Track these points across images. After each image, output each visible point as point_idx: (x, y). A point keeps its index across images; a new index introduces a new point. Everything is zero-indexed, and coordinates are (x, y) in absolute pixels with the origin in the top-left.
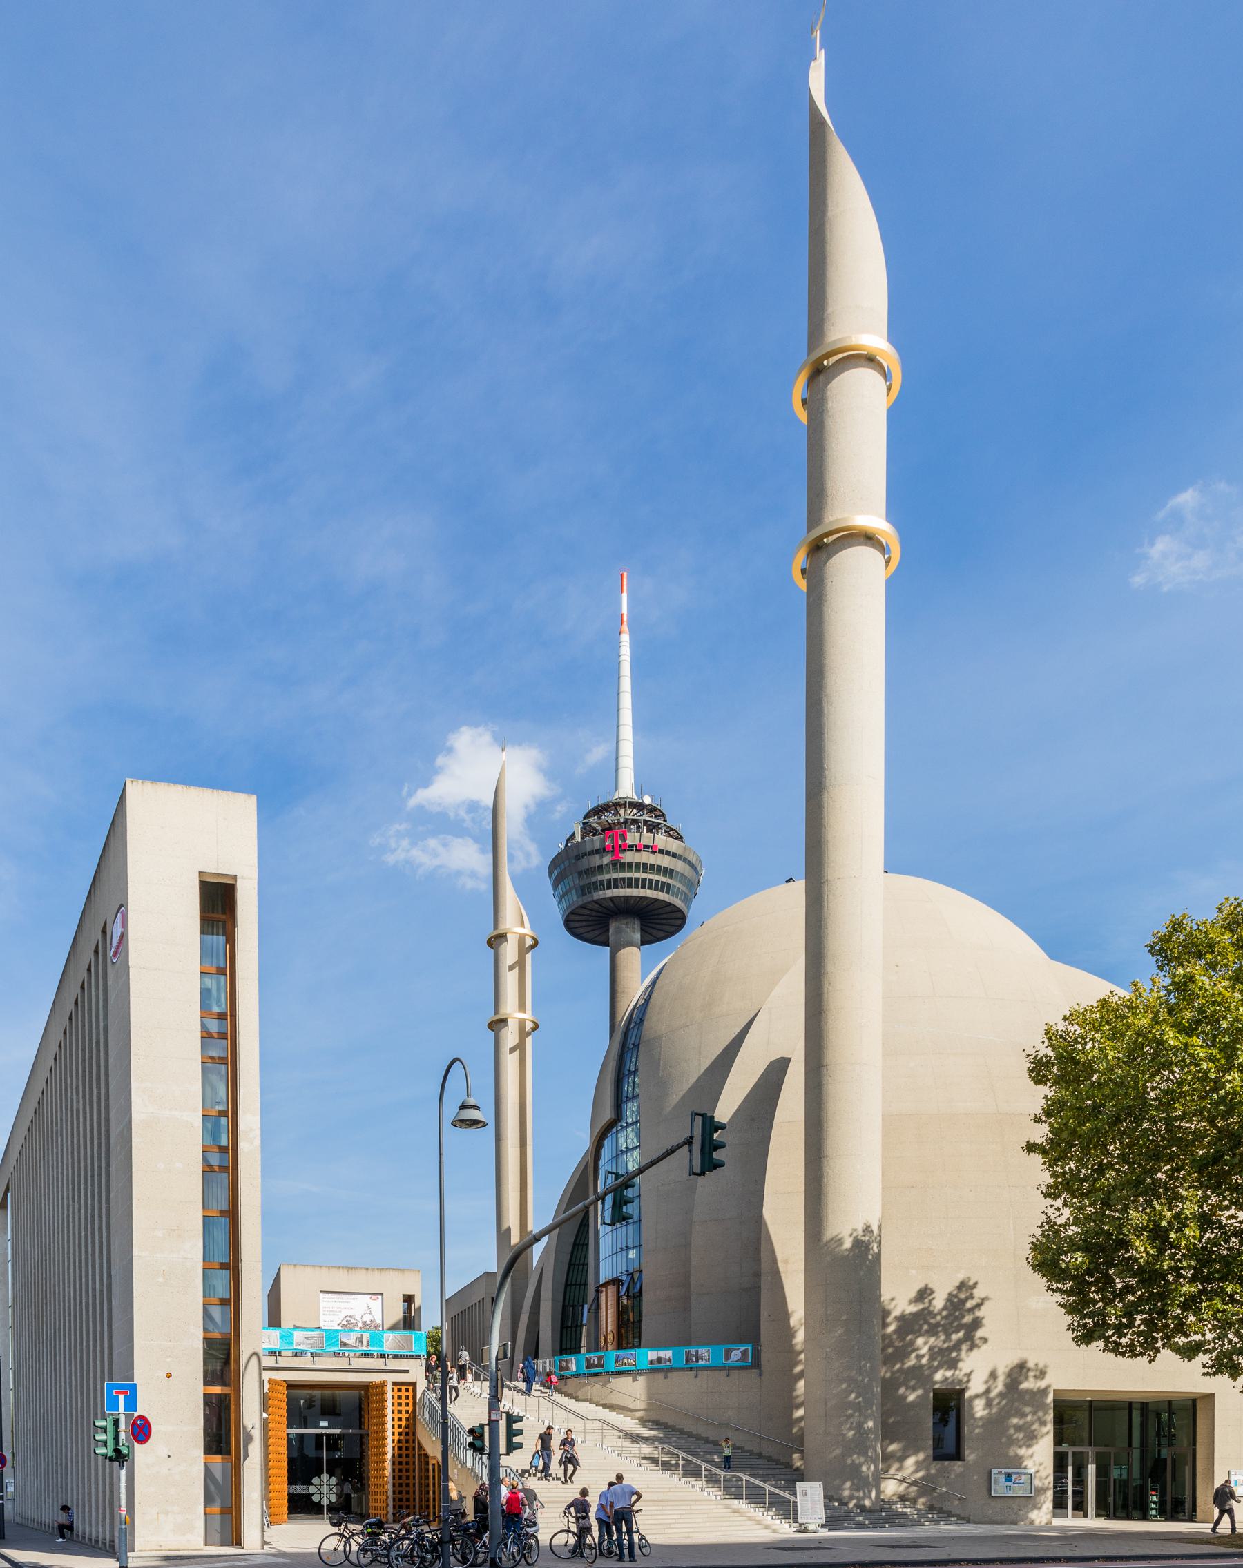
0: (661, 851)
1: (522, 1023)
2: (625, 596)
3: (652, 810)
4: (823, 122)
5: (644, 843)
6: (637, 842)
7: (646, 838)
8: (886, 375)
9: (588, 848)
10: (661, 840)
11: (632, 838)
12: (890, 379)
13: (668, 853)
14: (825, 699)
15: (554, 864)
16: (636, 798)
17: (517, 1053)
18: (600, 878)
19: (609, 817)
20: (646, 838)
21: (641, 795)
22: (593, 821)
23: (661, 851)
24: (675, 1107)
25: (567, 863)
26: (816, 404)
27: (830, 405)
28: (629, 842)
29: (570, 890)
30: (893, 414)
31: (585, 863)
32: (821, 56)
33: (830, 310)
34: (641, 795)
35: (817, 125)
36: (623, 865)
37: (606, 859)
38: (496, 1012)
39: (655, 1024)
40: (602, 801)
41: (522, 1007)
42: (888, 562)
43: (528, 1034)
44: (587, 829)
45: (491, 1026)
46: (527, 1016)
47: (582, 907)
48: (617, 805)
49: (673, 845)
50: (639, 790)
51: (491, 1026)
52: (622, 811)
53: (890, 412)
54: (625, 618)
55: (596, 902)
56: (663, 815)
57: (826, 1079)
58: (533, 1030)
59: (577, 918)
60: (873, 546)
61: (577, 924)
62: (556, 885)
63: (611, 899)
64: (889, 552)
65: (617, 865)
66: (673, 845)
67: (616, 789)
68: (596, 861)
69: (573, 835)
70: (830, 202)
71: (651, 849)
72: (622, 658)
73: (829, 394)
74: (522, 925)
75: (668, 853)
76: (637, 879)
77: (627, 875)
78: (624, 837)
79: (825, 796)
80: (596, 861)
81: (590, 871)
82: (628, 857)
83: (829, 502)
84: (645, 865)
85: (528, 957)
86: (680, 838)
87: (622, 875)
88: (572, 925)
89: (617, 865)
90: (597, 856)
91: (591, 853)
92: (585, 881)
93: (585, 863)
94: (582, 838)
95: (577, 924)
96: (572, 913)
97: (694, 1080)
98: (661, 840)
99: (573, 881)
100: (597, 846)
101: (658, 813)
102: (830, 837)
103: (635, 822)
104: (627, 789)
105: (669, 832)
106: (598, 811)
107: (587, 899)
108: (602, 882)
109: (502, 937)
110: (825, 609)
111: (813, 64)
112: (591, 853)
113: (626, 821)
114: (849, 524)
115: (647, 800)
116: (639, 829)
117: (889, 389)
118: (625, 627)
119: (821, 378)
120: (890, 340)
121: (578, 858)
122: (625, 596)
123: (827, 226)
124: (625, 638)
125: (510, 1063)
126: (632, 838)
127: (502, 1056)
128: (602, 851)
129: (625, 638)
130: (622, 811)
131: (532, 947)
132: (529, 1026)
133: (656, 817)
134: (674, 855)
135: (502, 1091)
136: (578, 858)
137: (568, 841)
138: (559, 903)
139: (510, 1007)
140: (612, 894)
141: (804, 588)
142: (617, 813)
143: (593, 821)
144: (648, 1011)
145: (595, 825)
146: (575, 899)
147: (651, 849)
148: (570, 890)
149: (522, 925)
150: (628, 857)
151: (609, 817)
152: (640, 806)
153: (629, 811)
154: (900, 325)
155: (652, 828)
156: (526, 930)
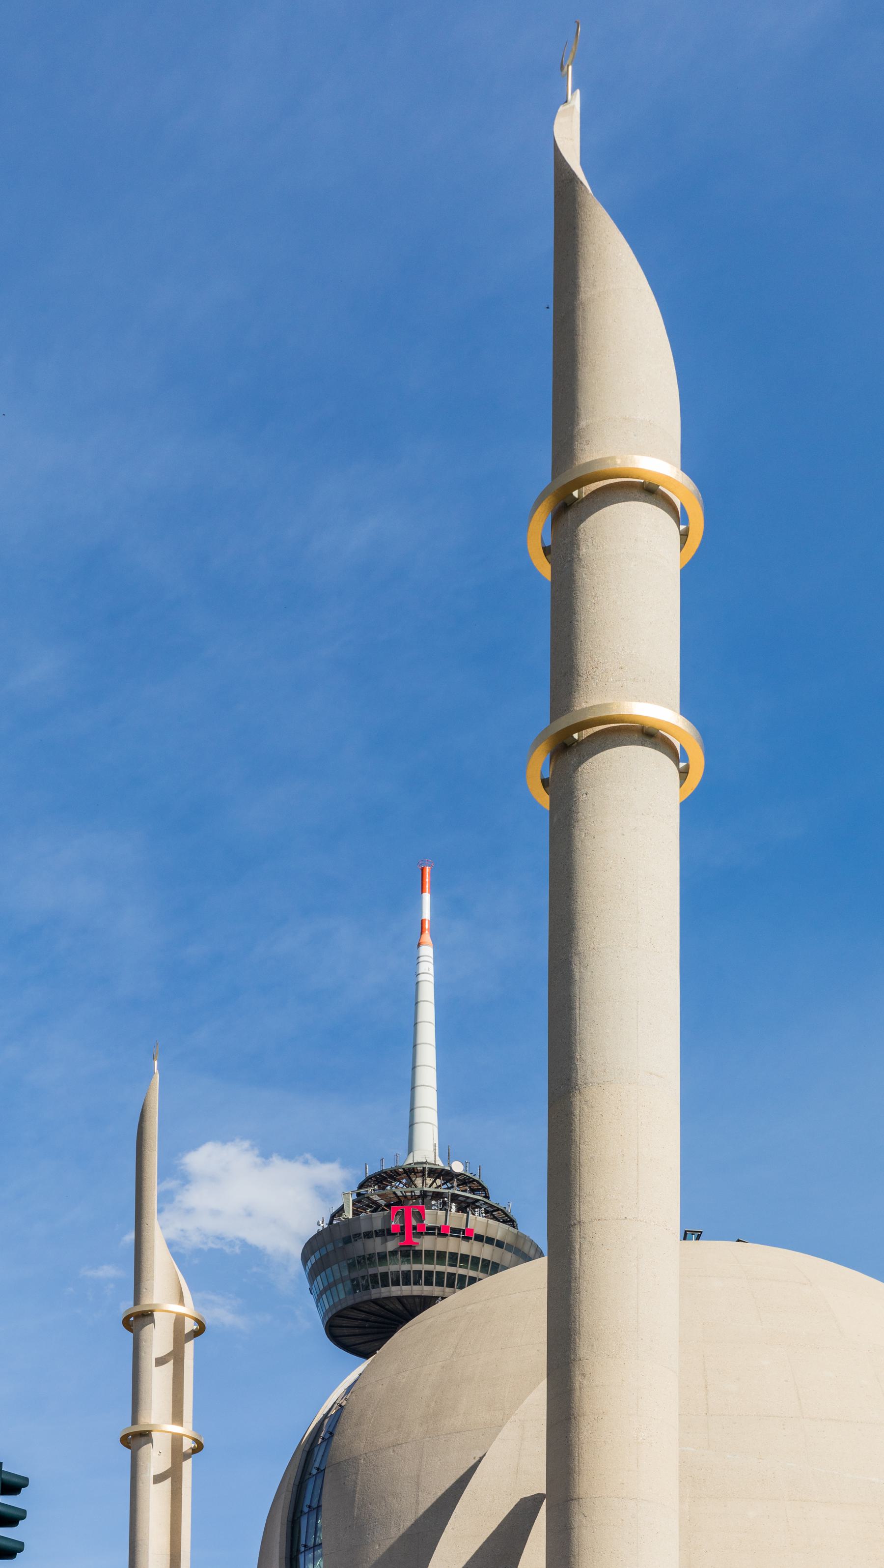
0: (479, 1238)
1: (177, 1440)
2: (427, 897)
3: (465, 1181)
4: (572, 178)
5: (452, 1224)
6: (440, 1223)
7: (455, 1218)
8: (678, 515)
9: (364, 1228)
10: (478, 1222)
11: (433, 1217)
12: (686, 521)
13: (490, 1241)
14: (576, 959)
15: (311, 1247)
16: (440, 1164)
17: (167, 1483)
18: (382, 1269)
19: (399, 1188)
20: (455, 1218)
21: (449, 1159)
22: (373, 1193)
23: (479, 1238)
24: (379, 1562)
25: (330, 1247)
26: (563, 552)
27: (583, 550)
28: (428, 1221)
29: (335, 1283)
30: (692, 577)
31: (359, 1248)
32: (575, 100)
33: (583, 424)
34: (449, 1159)
35: (564, 181)
36: (417, 1255)
37: (392, 1245)
38: (135, 1421)
39: (351, 1441)
40: (388, 1166)
41: (177, 1416)
42: (684, 774)
43: (186, 1456)
44: (362, 1203)
45: (126, 1440)
46: (186, 1429)
47: (353, 1308)
48: (410, 1172)
49: (499, 1230)
50: (447, 1153)
51: (126, 1440)
52: (419, 1181)
53: (687, 573)
54: (427, 926)
55: (375, 1302)
56: (484, 1189)
57: (578, 1520)
58: (195, 1451)
59: (345, 1322)
60: (655, 746)
61: (346, 1331)
62: (312, 1275)
63: (399, 1299)
64: (686, 758)
65: (409, 1253)
66: (499, 1230)
67: (410, 1149)
68: (376, 1245)
69: (341, 1209)
70: (582, 282)
71: (466, 1235)
72: (421, 978)
73: (581, 536)
74: (181, 1301)
75: (490, 1241)
76: (440, 1274)
77: (425, 1267)
78: (421, 1216)
79: (577, 1100)
80: (376, 1245)
81: (369, 1259)
82: (426, 1243)
83: (582, 684)
84: (453, 1256)
85: (189, 1347)
86: (510, 1221)
87: (416, 1267)
88: (338, 1331)
89: (409, 1253)
90: (378, 1240)
91: (368, 1235)
92: (358, 1273)
93: (359, 1248)
94: (356, 1213)
95: (346, 1331)
96: (338, 1315)
97: (408, 1524)
98: (478, 1222)
99: (338, 1270)
100: (378, 1225)
101: (475, 1186)
102: (584, 1159)
103: (437, 1196)
104: (427, 1148)
105: (492, 1212)
106: (382, 1179)
107: (361, 1296)
108: (385, 1275)
109: (146, 1316)
110: (576, 832)
111: (561, 108)
112: (368, 1235)
113: (424, 1194)
114: (614, 712)
115: (457, 1167)
116: (444, 1207)
117: (684, 536)
118: (427, 937)
119: (571, 515)
120: (684, 468)
121: (347, 1240)
122: (427, 897)
123: (580, 313)
124: (427, 951)
125: (155, 1499)
126: (433, 1217)
127: (141, 1486)
128: (386, 1233)
129: (427, 951)
130: (419, 1181)
131: (196, 1334)
132: (188, 1445)
133: (473, 1191)
134: (500, 1244)
135: (141, 1535)
136: (347, 1240)
137: (333, 1217)
138: (318, 1301)
139: (157, 1412)
140: (371, 1280)
141: (547, 806)
142: (411, 1183)
143: (373, 1193)
144: (341, 1421)
145: (376, 1198)
146: (343, 1296)
147: (466, 1235)
148: (335, 1283)
149: (181, 1301)
150: (426, 1243)
151: (399, 1188)
152: (447, 1175)
153: (429, 1181)
154: (699, 450)
155: (465, 1206)
156: (187, 1309)
